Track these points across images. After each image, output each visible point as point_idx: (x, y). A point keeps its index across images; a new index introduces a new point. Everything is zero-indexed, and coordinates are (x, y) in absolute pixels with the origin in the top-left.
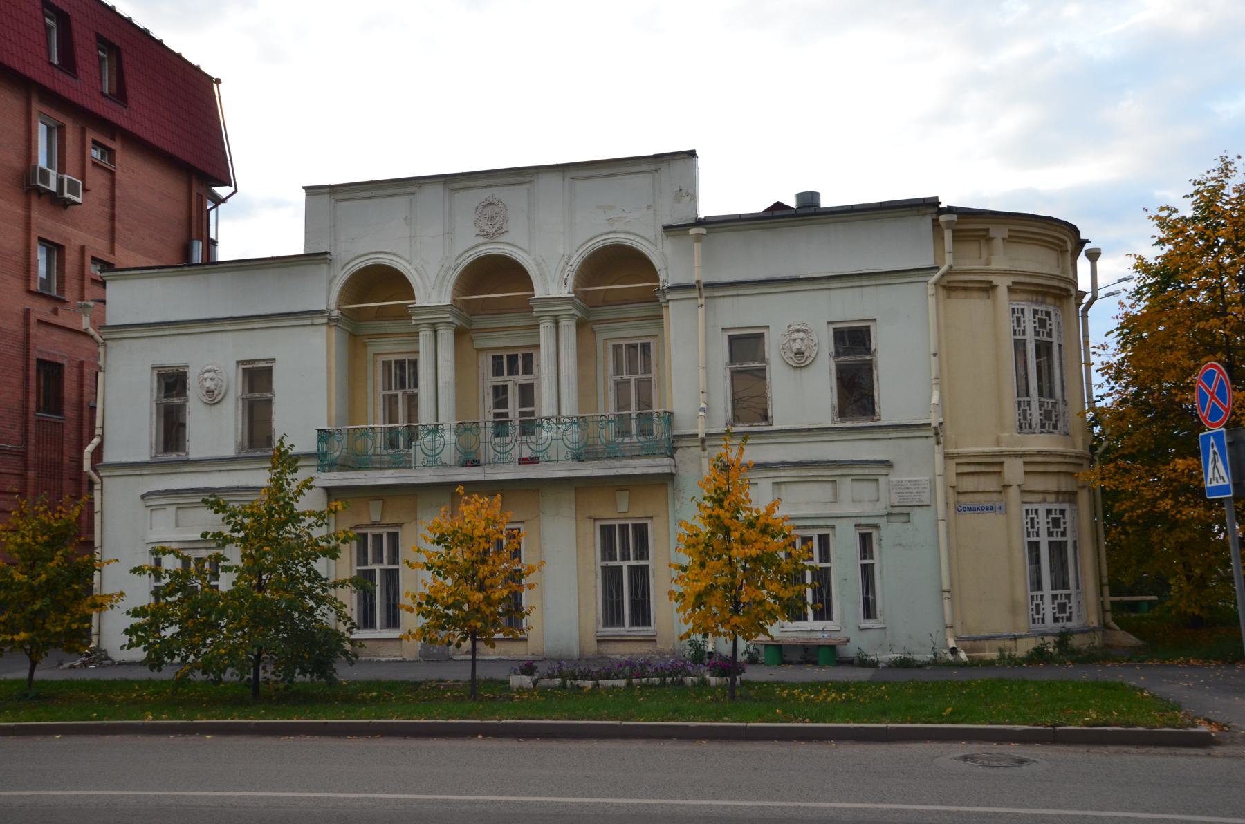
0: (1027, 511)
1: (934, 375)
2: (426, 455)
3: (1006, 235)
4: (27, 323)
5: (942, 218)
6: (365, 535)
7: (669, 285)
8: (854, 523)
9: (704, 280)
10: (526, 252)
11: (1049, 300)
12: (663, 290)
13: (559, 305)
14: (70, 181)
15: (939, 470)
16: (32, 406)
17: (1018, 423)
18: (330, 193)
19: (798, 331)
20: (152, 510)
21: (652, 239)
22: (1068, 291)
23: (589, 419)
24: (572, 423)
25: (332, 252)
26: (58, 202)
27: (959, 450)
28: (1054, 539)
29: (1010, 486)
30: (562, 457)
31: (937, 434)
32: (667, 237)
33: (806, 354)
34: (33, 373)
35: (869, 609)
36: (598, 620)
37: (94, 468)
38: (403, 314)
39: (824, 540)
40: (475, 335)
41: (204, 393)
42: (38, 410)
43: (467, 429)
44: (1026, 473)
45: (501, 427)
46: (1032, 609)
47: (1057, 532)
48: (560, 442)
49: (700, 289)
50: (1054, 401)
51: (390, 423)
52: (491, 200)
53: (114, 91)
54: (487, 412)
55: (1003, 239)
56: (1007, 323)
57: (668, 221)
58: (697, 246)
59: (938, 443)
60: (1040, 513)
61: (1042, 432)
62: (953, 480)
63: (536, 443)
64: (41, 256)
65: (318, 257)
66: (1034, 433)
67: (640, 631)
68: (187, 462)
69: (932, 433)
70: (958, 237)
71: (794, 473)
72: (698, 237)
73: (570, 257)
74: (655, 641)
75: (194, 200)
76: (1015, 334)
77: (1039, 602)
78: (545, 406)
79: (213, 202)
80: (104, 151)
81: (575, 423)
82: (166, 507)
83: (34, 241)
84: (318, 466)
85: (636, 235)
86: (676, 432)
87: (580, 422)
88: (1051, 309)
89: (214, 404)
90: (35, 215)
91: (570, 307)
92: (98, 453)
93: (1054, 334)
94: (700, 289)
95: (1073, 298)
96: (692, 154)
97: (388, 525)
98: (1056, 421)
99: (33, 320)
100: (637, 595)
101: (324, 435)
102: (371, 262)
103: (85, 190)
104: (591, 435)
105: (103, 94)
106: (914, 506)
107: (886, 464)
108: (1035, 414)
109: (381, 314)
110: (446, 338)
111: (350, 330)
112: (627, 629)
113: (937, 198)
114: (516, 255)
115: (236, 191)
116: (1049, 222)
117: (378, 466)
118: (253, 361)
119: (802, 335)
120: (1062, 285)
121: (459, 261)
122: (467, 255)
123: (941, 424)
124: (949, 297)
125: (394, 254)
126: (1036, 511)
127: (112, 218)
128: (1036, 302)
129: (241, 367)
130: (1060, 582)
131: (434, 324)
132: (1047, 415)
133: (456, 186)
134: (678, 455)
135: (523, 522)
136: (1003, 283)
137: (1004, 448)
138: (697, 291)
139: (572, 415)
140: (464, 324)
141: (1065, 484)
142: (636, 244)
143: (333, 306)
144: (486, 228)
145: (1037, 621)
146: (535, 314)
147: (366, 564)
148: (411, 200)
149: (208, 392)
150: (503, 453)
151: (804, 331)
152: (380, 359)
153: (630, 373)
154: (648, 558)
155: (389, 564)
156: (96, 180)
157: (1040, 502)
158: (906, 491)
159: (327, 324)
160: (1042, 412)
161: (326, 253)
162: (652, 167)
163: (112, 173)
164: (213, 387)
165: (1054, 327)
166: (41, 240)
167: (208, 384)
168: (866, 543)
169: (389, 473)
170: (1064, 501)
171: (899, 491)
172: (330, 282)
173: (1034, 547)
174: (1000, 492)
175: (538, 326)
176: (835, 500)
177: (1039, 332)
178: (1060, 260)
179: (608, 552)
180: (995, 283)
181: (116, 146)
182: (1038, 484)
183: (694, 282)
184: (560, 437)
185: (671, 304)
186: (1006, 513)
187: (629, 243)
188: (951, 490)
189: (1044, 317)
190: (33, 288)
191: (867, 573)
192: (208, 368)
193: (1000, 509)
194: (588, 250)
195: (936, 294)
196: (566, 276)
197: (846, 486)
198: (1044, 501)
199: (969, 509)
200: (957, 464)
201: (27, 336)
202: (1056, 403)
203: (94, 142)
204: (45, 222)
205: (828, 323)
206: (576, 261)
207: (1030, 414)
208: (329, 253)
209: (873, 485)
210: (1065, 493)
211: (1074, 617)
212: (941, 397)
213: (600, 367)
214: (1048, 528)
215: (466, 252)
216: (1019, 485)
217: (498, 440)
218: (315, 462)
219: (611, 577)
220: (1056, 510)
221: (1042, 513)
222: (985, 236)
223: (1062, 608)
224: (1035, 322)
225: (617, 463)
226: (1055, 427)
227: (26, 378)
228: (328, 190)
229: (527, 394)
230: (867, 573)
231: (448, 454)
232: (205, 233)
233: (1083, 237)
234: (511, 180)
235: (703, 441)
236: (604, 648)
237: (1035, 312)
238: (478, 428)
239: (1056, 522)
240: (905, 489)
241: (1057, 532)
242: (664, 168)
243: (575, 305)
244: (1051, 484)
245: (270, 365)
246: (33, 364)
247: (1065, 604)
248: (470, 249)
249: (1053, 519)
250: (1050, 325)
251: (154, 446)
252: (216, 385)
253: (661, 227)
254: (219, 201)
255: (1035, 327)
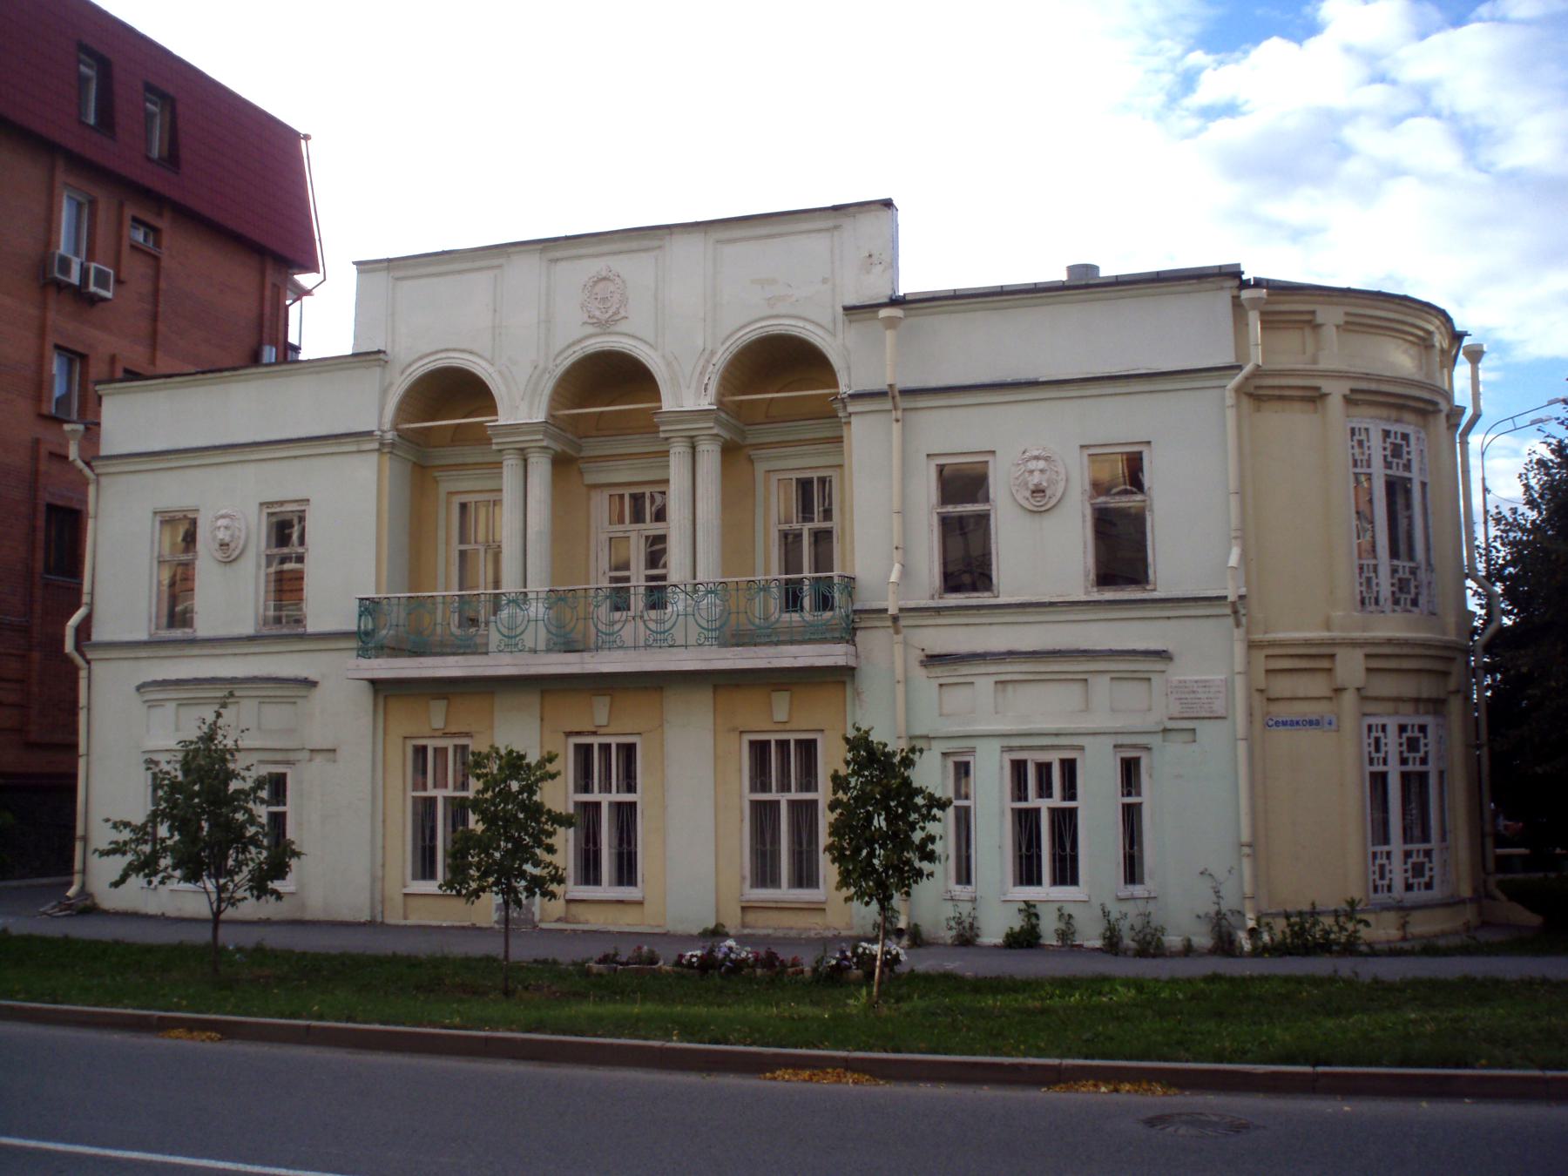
0: (1370, 728)
1: (1233, 526)
2: (703, 628)
3: (1341, 319)
4: (35, 458)
5: (1246, 294)
6: (424, 748)
7: (851, 392)
8: (1113, 743)
9: (900, 385)
10: (651, 346)
11: (1408, 416)
12: (843, 399)
13: (695, 421)
14: (99, 272)
15: (1239, 665)
16: (39, 566)
17: (1358, 598)
18: (388, 269)
19: (1037, 458)
20: (149, 707)
21: (830, 326)
22: (1435, 404)
23: (732, 587)
24: (709, 592)
25: (389, 350)
26: (82, 297)
27: (1271, 636)
28: (1410, 768)
29: (1345, 689)
30: (692, 640)
31: (1236, 612)
32: (850, 322)
33: (1048, 493)
34: (41, 521)
35: (1132, 870)
36: (743, 878)
37: (78, 647)
38: (480, 437)
39: (1069, 767)
40: (586, 465)
41: (217, 546)
42: (48, 570)
43: (560, 599)
44: (1369, 670)
45: (620, 600)
46: (1374, 873)
47: (1414, 758)
48: (690, 618)
49: (893, 398)
50: (1412, 564)
51: (461, 590)
52: (604, 274)
53: (165, 154)
54: (772, 570)
55: (1338, 327)
56: (1342, 450)
57: (852, 300)
58: (890, 335)
59: (1238, 625)
60: (1389, 729)
61: (1394, 611)
62: (1261, 681)
63: (659, 622)
64: (56, 366)
65: (368, 358)
66: (1383, 612)
67: (805, 894)
68: (193, 642)
69: (1228, 611)
70: (1270, 322)
71: (1024, 668)
72: (891, 323)
73: (713, 353)
74: (824, 910)
75: (268, 293)
76: (1355, 465)
77: (1385, 861)
78: (676, 568)
79: (295, 293)
80: (148, 230)
81: (711, 592)
82: (298, 700)
83: (49, 347)
84: (359, 649)
85: (805, 319)
86: (858, 606)
87: (720, 589)
88: (1409, 429)
89: (230, 562)
90: (52, 315)
91: (711, 425)
92: (84, 629)
93: (1415, 466)
94: (893, 398)
95: (1443, 416)
96: (888, 204)
97: (454, 735)
98: (1417, 594)
99: (43, 451)
100: (800, 844)
101: (369, 607)
102: (440, 364)
103: (119, 281)
104: (734, 609)
105: (149, 159)
106: (1204, 718)
107: (1162, 655)
108: (1385, 585)
109: (459, 436)
110: (540, 469)
111: (415, 460)
112: (785, 892)
113: (1239, 265)
114: (638, 351)
115: (325, 280)
116: (1403, 302)
117: (438, 650)
118: (282, 503)
119: (1041, 464)
120: (1426, 395)
121: (558, 361)
122: (570, 351)
123: (1241, 597)
124: (1258, 410)
125: (471, 353)
126: (1384, 728)
127: (155, 318)
128: (1388, 419)
129: (266, 511)
130: (1417, 828)
131: (522, 449)
132: (1402, 586)
133: (558, 254)
134: (860, 635)
135: (639, 734)
136: (1336, 390)
137: (1336, 634)
138: (890, 399)
139: (707, 580)
140: (566, 449)
141: (1427, 688)
142: (807, 333)
143: (387, 426)
144: (597, 313)
145: (1380, 888)
146: (662, 435)
147: (425, 788)
148: (496, 276)
149: (221, 545)
150: (661, 633)
151: (1046, 459)
152: (457, 500)
153: (805, 520)
154: (816, 790)
155: (455, 789)
156: (135, 268)
157: (1389, 715)
158: (1192, 696)
159: (378, 450)
160: (1395, 581)
161: (379, 352)
162: (830, 223)
163: (156, 259)
164: (227, 539)
165: (1414, 457)
166: (58, 347)
167: (221, 535)
168: (1130, 771)
169: (451, 660)
170: (1427, 713)
171: (1179, 696)
172: (384, 392)
173: (1380, 780)
174: (1330, 699)
175: (666, 453)
176: (1087, 709)
177: (1391, 463)
178: (1424, 361)
179: (760, 780)
180: (1325, 390)
181: (163, 224)
182: (1388, 686)
183: (884, 387)
184: (689, 610)
185: (853, 419)
186: (1338, 731)
187: (795, 332)
188: (1257, 696)
189: (1399, 441)
190: (45, 411)
191: (1131, 817)
192: (223, 512)
193: (1330, 723)
194: (738, 343)
195: (1238, 405)
196: (706, 381)
197: (1101, 685)
198: (1396, 713)
199: (1284, 723)
200: (1267, 656)
201: (36, 473)
202: (1417, 568)
203: (135, 220)
204: (64, 324)
205: (1082, 447)
206: (722, 356)
207: (1377, 584)
208: (384, 352)
209: (1142, 686)
210: (1428, 700)
211: (1436, 882)
212: (1244, 556)
213: (759, 511)
214: (1401, 752)
215: (569, 346)
216: (1359, 689)
217: (617, 615)
218: (353, 644)
219: (764, 814)
220: (1413, 726)
221: (1392, 730)
222: (1309, 322)
223: (1418, 870)
224: (1385, 449)
225: (771, 650)
226: (1415, 603)
227: (34, 529)
228: (386, 264)
229: (656, 552)
230: (1131, 817)
231: (537, 636)
232: (281, 337)
233: (1459, 328)
234: (634, 245)
235: (895, 619)
236: (751, 917)
237: (1387, 434)
238: (574, 597)
239: (1413, 745)
240: (1189, 693)
241: (1414, 758)
242: (846, 223)
243: (718, 421)
244: (1406, 687)
245: (303, 508)
246: (42, 508)
247: (1423, 864)
248: (574, 344)
249: (1409, 739)
250: (1408, 453)
251: (154, 620)
252: (232, 536)
253: (841, 309)
254: (302, 293)
255: (1385, 456)
